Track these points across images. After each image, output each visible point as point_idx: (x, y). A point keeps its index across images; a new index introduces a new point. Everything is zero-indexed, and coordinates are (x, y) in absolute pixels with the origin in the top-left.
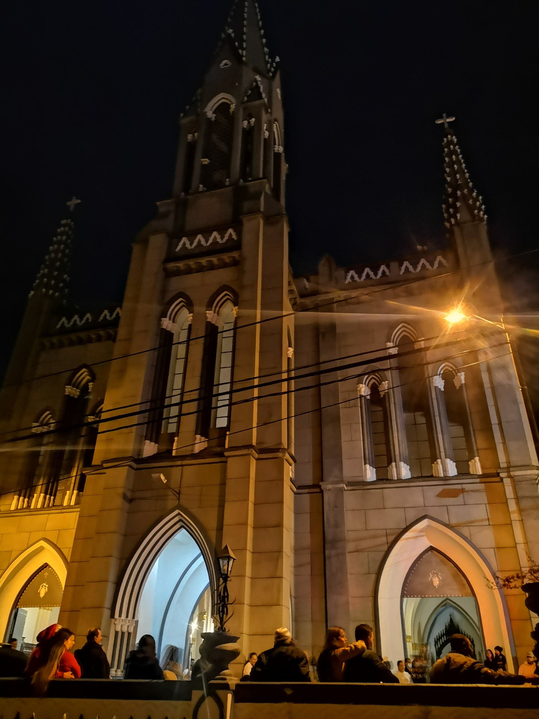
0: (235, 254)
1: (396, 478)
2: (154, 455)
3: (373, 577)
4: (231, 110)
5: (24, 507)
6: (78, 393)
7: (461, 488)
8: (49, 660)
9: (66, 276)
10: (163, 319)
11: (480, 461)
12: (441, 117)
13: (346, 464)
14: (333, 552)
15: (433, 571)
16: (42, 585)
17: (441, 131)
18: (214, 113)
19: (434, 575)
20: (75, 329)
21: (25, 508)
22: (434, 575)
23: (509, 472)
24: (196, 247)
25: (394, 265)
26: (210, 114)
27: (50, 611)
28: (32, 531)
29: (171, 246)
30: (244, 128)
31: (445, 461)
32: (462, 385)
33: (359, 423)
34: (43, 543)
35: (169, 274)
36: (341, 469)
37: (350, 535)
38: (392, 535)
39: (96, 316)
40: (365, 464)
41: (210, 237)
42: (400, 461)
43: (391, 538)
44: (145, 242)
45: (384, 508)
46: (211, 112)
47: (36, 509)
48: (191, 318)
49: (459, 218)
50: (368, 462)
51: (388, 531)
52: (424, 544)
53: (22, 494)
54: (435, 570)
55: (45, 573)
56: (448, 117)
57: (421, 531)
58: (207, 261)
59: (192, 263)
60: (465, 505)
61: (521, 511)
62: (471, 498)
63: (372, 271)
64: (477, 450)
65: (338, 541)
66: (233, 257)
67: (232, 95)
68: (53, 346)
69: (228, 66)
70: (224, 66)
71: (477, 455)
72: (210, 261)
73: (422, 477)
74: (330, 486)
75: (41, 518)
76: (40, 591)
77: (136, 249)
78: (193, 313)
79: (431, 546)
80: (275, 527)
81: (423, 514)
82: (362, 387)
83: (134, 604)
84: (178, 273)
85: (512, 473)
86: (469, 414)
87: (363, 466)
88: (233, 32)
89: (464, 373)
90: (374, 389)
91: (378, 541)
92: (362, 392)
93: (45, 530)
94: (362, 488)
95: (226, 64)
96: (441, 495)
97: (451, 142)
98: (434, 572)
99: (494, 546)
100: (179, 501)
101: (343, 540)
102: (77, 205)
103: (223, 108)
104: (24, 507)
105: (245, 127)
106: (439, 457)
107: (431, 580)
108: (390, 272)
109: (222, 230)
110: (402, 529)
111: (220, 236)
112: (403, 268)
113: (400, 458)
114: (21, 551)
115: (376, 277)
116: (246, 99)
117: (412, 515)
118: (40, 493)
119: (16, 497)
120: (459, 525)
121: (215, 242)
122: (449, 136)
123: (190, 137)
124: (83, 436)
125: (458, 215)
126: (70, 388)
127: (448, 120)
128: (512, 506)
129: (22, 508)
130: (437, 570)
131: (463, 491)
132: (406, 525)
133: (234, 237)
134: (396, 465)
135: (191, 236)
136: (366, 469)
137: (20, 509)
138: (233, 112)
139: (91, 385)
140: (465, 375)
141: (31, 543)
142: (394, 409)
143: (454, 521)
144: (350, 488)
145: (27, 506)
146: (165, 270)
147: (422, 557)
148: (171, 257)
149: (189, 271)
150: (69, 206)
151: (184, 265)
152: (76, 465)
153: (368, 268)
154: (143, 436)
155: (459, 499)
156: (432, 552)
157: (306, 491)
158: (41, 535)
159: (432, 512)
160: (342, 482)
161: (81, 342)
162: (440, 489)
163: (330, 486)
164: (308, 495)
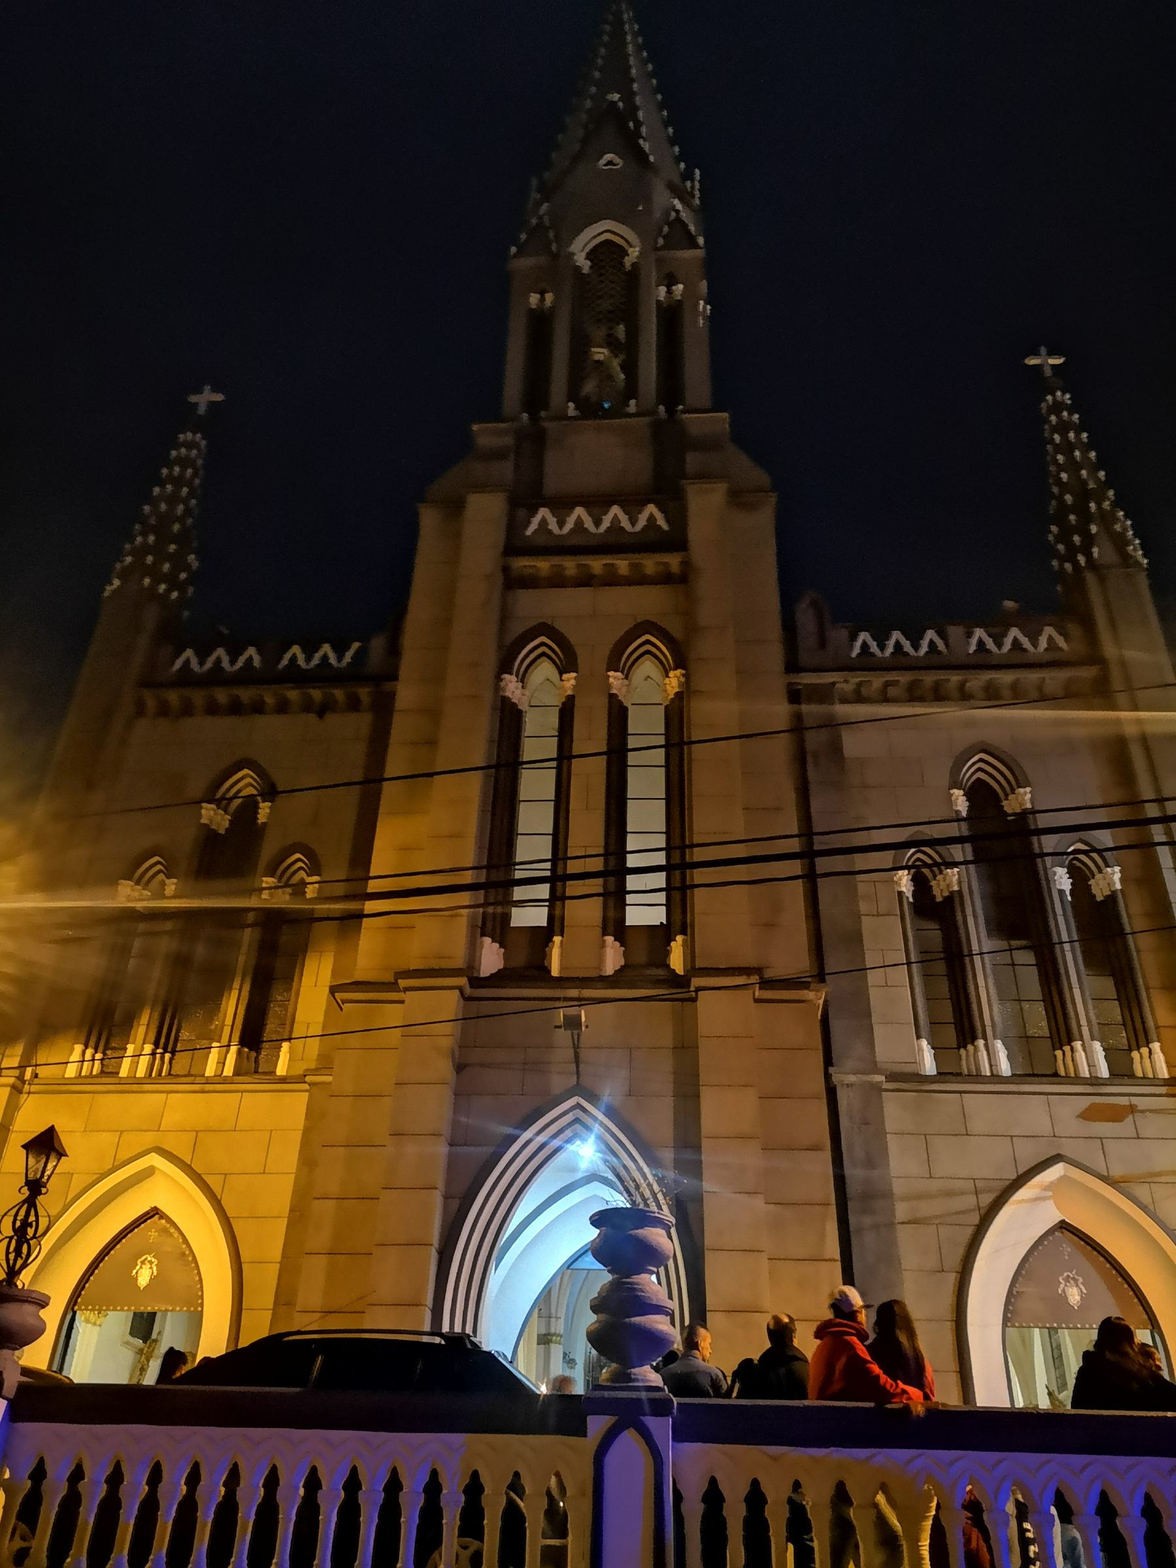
0: (674, 561)
1: (988, 1074)
2: (499, 970)
3: (952, 1278)
4: (628, 262)
5: (94, 1073)
6: (227, 824)
7: (1127, 1103)
8: (1122, 1322)
9: (192, 557)
10: (506, 676)
12: (1036, 354)
14: (867, 1220)
15: (1065, 1274)
16: (143, 1258)
17: (1037, 381)
18: (587, 258)
19: (1069, 1282)
20: (217, 677)
21: (96, 1076)
22: (1069, 1282)
24: (572, 531)
25: (955, 632)
26: (582, 262)
27: (97, 1329)
28: (123, 1131)
29: (514, 527)
30: (658, 302)
31: (1091, 1046)
32: (1114, 893)
34: (155, 1160)
35: (513, 582)
37: (898, 1187)
38: (989, 1191)
39: (272, 655)
40: (919, 1037)
41: (605, 514)
42: (995, 1038)
43: (987, 1199)
44: (455, 507)
45: (967, 1135)
46: (583, 254)
47: (133, 1080)
48: (573, 682)
49: (1096, 555)
51: (979, 1184)
52: (1050, 1215)
53: (92, 1043)
54: (1071, 1273)
55: (150, 1231)
56: (1051, 353)
58: (605, 565)
59: (570, 565)
60: (1138, 1138)
63: (907, 639)
64: (1157, 1027)
65: (879, 1195)
66: (666, 564)
67: (632, 227)
68: (164, 710)
69: (619, 167)
70: (605, 165)
71: (1155, 1038)
72: (612, 565)
73: (1034, 1075)
74: (852, 1078)
75: (150, 1101)
76: (137, 1273)
77: (429, 520)
78: (577, 672)
80: (809, 1150)
81: (1054, 1153)
83: (482, 1301)
84: (530, 582)
86: (1135, 954)
88: (620, 99)
89: (1120, 868)
90: (921, 883)
91: (959, 1203)
92: (902, 885)
93: (158, 1130)
94: (919, 1088)
95: (610, 163)
96: (1088, 1115)
97: (1057, 407)
98: (1068, 1276)
100: (578, 1078)
101: (889, 1195)
102: (212, 405)
103: (606, 253)
104: (94, 1073)
105: (662, 298)
106: (1078, 1037)
107: (1064, 1291)
108: (947, 645)
109: (632, 504)
110: (1009, 1180)
111: (555, 519)
112: (974, 641)
114: (96, 1176)
115: (1000, 650)
116: (661, 241)
117: (1028, 1155)
118: (144, 1043)
119: (78, 1048)
121: (615, 526)
122: (1059, 393)
123: (534, 299)
124: (249, 926)
125: (1095, 551)
126: (212, 809)
127: (1052, 361)
129: (91, 1076)
130: (1074, 1273)
131: (1132, 1109)
132: (1017, 1172)
133: (661, 522)
135: (562, 505)
136: (921, 1049)
137: (86, 1077)
138: (634, 265)
139: (264, 810)
140: (1121, 872)
141: (124, 1155)
143: (1116, 1172)
145: (99, 1072)
146: (506, 569)
148: (514, 546)
149: (557, 581)
150: (196, 404)
151: (552, 566)
152: (236, 985)
153: (867, 633)
154: (477, 926)
155: (1126, 1127)
156: (1062, 1233)
158: (149, 1139)
161: (236, 708)
162: (1086, 1102)
163: (852, 1078)
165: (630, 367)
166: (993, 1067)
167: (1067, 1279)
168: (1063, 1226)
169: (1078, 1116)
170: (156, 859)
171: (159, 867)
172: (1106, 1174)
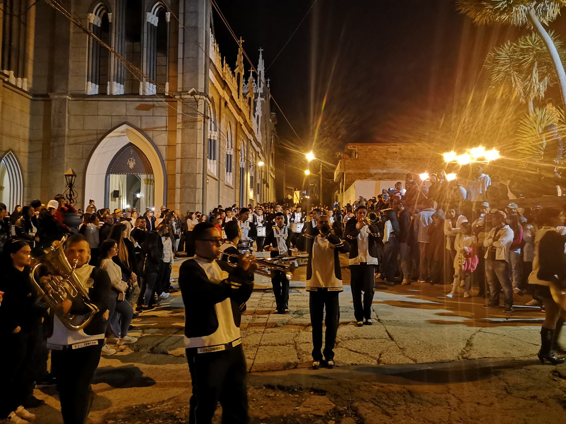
3: (85, 160)
11: (169, 84)
13: (72, 80)
14: (56, 144)
23: (181, 95)
33: (86, 47)
36: (67, 84)
40: (88, 81)
42: (114, 81)
43: (100, 136)
50: (90, 80)
52: (125, 141)
57: (122, 132)
61: (184, 122)
62: (158, 112)
64: (169, 77)
79: (130, 143)
81: (124, 121)
82: (92, 16)
85: (182, 96)
86: (168, 48)
91: (90, 138)
96: (139, 108)
99: (166, 144)
113: (114, 78)
117: (116, 121)
120: (147, 130)
134: (110, 83)
142: (114, 37)
143: (144, 127)
144: (73, 99)
147: (125, 149)
155: (150, 112)
157: (41, 98)
159: (130, 120)
160: (66, 94)
162: (138, 104)
163: (56, 97)
164: (42, 102)
165: (319, 196)
166: (206, 124)
167: (130, 160)
168: (130, 144)
169: (135, 109)
172: (140, 128)
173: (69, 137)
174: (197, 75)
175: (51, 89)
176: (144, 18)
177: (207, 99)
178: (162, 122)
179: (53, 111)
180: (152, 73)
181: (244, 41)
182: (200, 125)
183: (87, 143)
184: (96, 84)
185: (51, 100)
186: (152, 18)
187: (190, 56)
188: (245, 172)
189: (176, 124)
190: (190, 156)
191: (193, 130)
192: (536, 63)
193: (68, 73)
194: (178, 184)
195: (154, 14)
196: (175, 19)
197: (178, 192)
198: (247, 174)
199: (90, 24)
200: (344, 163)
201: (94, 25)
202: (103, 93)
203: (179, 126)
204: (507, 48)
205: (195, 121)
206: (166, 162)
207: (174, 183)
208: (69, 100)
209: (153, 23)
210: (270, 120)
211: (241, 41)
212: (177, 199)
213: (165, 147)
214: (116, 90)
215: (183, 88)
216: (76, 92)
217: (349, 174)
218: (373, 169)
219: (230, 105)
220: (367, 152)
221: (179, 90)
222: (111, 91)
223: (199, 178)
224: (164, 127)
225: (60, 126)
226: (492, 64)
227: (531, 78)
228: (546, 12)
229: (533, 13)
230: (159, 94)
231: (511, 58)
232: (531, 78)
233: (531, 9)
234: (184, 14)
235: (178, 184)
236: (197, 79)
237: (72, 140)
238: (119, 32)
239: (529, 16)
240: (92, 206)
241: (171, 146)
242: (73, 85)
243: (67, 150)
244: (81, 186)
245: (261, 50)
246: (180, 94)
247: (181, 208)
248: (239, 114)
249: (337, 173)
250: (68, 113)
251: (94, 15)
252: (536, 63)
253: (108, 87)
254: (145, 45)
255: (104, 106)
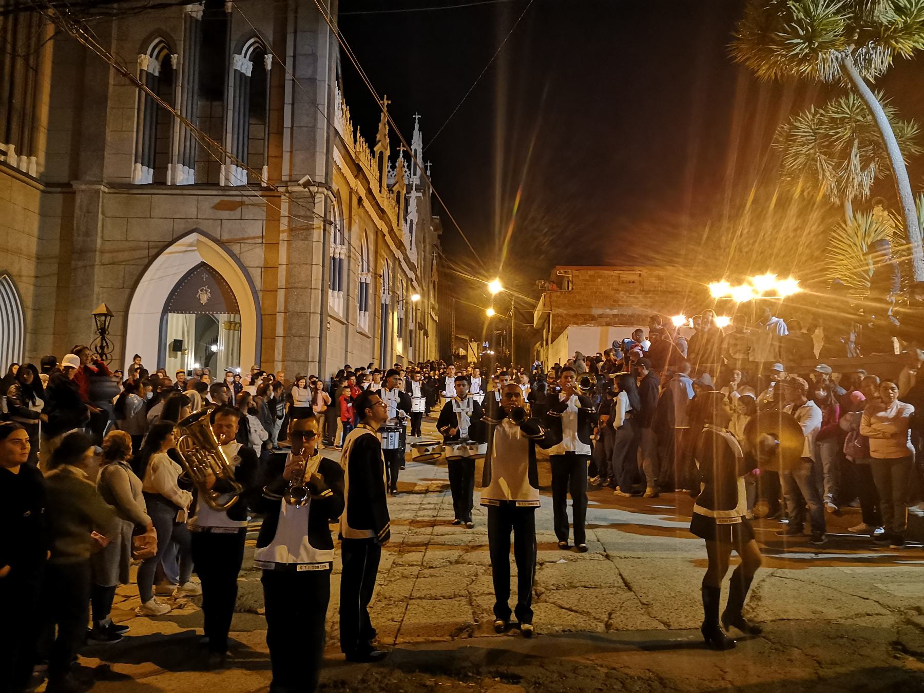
3: (128, 291)
14: (80, 264)
36: (102, 167)
38: (154, 247)
40: (136, 162)
42: (178, 162)
43: (154, 252)
52: (195, 259)
57: (191, 245)
61: (291, 230)
62: (249, 213)
64: (268, 157)
74: (83, 187)
82: (145, 59)
87: (133, 165)
91: (137, 254)
96: (219, 207)
117: (180, 227)
120: (229, 242)
128: (284, 224)
143: (225, 237)
144: (111, 191)
155: (237, 214)
157: (59, 189)
159: (204, 226)
160: (100, 182)
162: (217, 200)
163: (83, 187)
167: (201, 291)
168: (203, 264)
170: (252, 40)
171: (162, 45)
173: (102, 252)
174: (313, 155)
175: (75, 174)
176: (230, 63)
177: (330, 193)
178: (256, 229)
179: (77, 212)
180: (240, 151)
181: (390, 102)
182: (317, 235)
183: (132, 262)
184: (149, 167)
185: (74, 193)
186: (242, 64)
187: (302, 125)
188: (390, 311)
189: (279, 232)
190: (300, 285)
191: (306, 242)
192: (856, 141)
193: (103, 150)
194: (280, 330)
195: (245, 57)
196: (279, 66)
197: (280, 342)
198: (393, 314)
199: (141, 70)
200: (550, 297)
201: (148, 74)
202: (159, 182)
203: (284, 236)
204: (810, 117)
205: (310, 228)
206: (260, 295)
207: (274, 329)
208: (105, 192)
209: (243, 71)
210: (431, 228)
211: (386, 102)
212: (278, 354)
213: (259, 270)
214: (182, 177)
215: (290, 176)
216: (118, 181)
217: (558, 315)
218: (597, 307)
219: (366, 203)
220: (587, 280)
221: (284, 178)
222: (173, 179)
223: (315, 320)
224: (258, 238)
225: (87, 234)
226: (785, 143)
227: (848, 166)
228: (870, 61)
229: (849, 62)
230: (250, 184)
231: (815, 133)
232: (848, 166)
233: (847, 56)
234: (294, 57)
235: (280, 330)
236: (314, 161)
237: (107, 258)
238: (188, 84)
239: (843, 67)
240: (137, 366)
241: (269, 268)
242: (111, 168)
243: (99, 273)
244: (119, 333)
245: (417, 117)
246: (286, 184)
247: (285, 369)
248: (381, 218)
249: (538, 314)
250: (103, 214)
251: (148, 56)
252: (856, 141)
253: (169, 173)
254: (231, 106)
255: (162, 204)
